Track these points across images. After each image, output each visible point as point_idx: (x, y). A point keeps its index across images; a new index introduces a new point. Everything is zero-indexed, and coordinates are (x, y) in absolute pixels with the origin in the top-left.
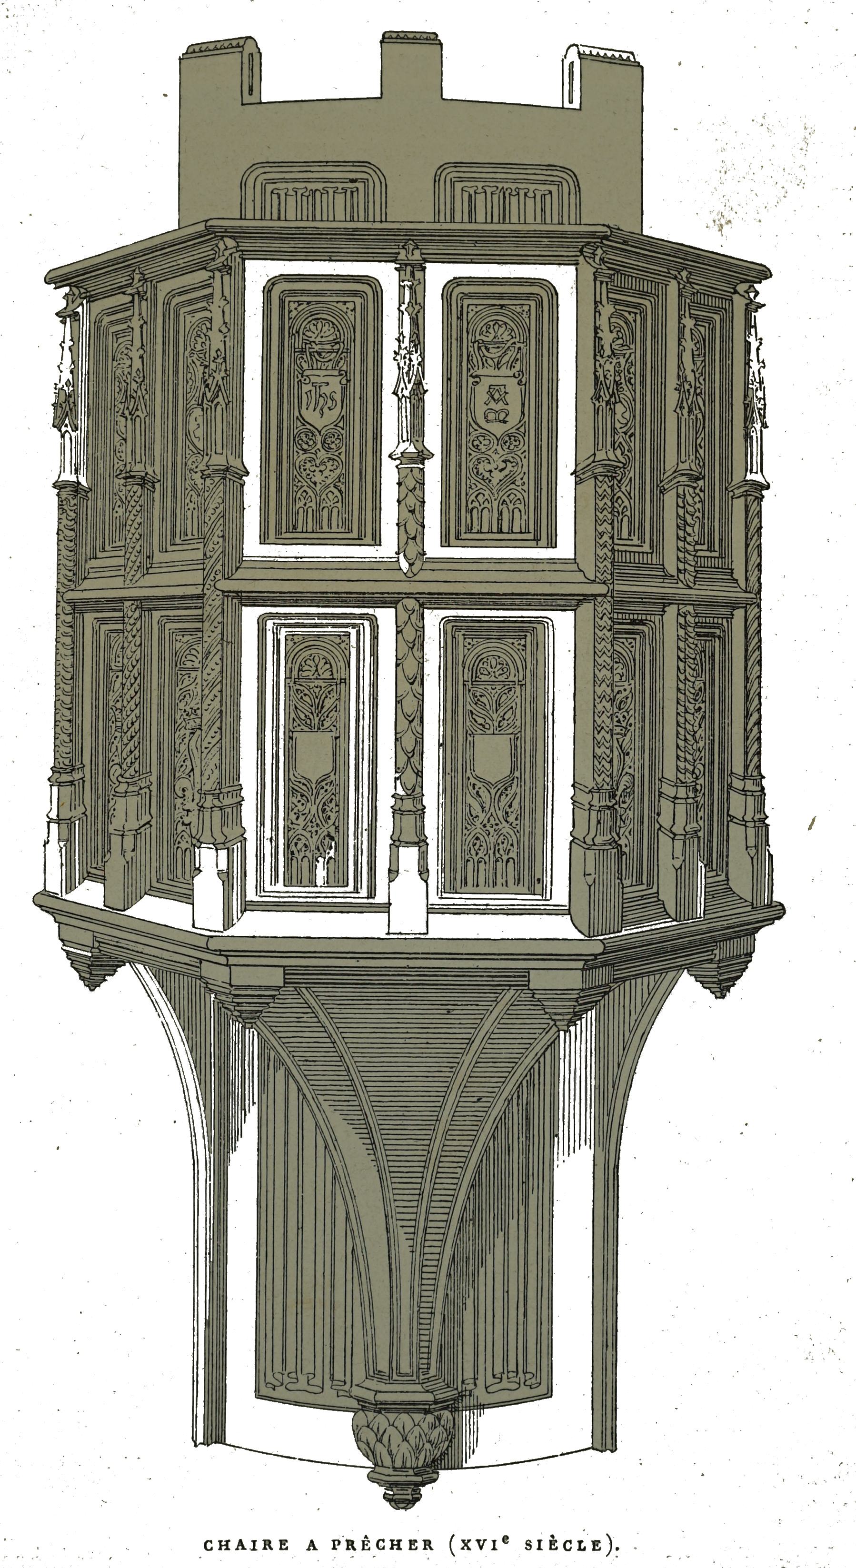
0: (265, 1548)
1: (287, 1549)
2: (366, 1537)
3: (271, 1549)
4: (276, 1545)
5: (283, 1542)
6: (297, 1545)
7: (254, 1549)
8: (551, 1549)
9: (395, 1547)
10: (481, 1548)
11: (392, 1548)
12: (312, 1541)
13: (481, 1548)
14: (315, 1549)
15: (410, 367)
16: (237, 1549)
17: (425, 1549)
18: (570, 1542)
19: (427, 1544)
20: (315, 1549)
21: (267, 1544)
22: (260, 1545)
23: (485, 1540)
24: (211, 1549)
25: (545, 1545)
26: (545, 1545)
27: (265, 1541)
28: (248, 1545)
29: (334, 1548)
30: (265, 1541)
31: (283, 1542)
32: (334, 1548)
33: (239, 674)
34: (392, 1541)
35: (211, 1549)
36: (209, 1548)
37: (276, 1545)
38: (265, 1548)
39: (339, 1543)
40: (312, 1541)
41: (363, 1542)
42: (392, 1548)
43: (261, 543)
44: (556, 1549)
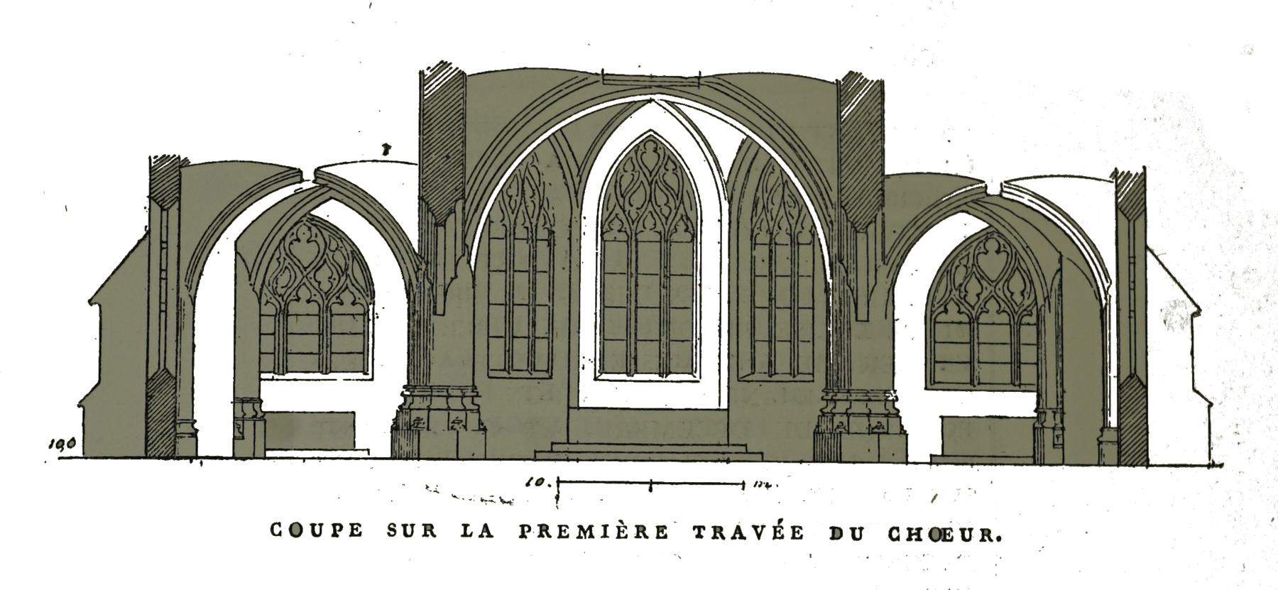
0: (425, 535)
1: (665, 537)
2: (780, 521)
3: (646, 537)
4: (652, 532)
5: (661, 529)
6: (875, 535)
7: (605, 536)
8: (658, 537)
9: (914, 537)
10: (759, 536)
11: (909, 539)
12: (486, 526)
13: (759, 536)
14: (490, 536)
15: (325, 313)
16: (481, 536)
17: (983, 540)
18: (898, 529)
19: (429, 529)
20: (490, 536)
21: (641, 531)
22: (598, 531)
23: (763, 527)
24: (280, 534)
25: (612, 531)
26: (612, 531)
27: (637, 527)
28: (748, 531)
29: (523, 536)
30: (637, 527)
31: (661, 529)
32: (523, 536)
33: (411, 336)
34: (910, 529)
35: (280, 534)
36: (276, 532)
37: (652, 532)
38: (638, 536)
39: (530, 529)
40: (486, 526)
41: (775, 528)
42: (909, 539)
43: (926, 388)
44: (782, 537)
